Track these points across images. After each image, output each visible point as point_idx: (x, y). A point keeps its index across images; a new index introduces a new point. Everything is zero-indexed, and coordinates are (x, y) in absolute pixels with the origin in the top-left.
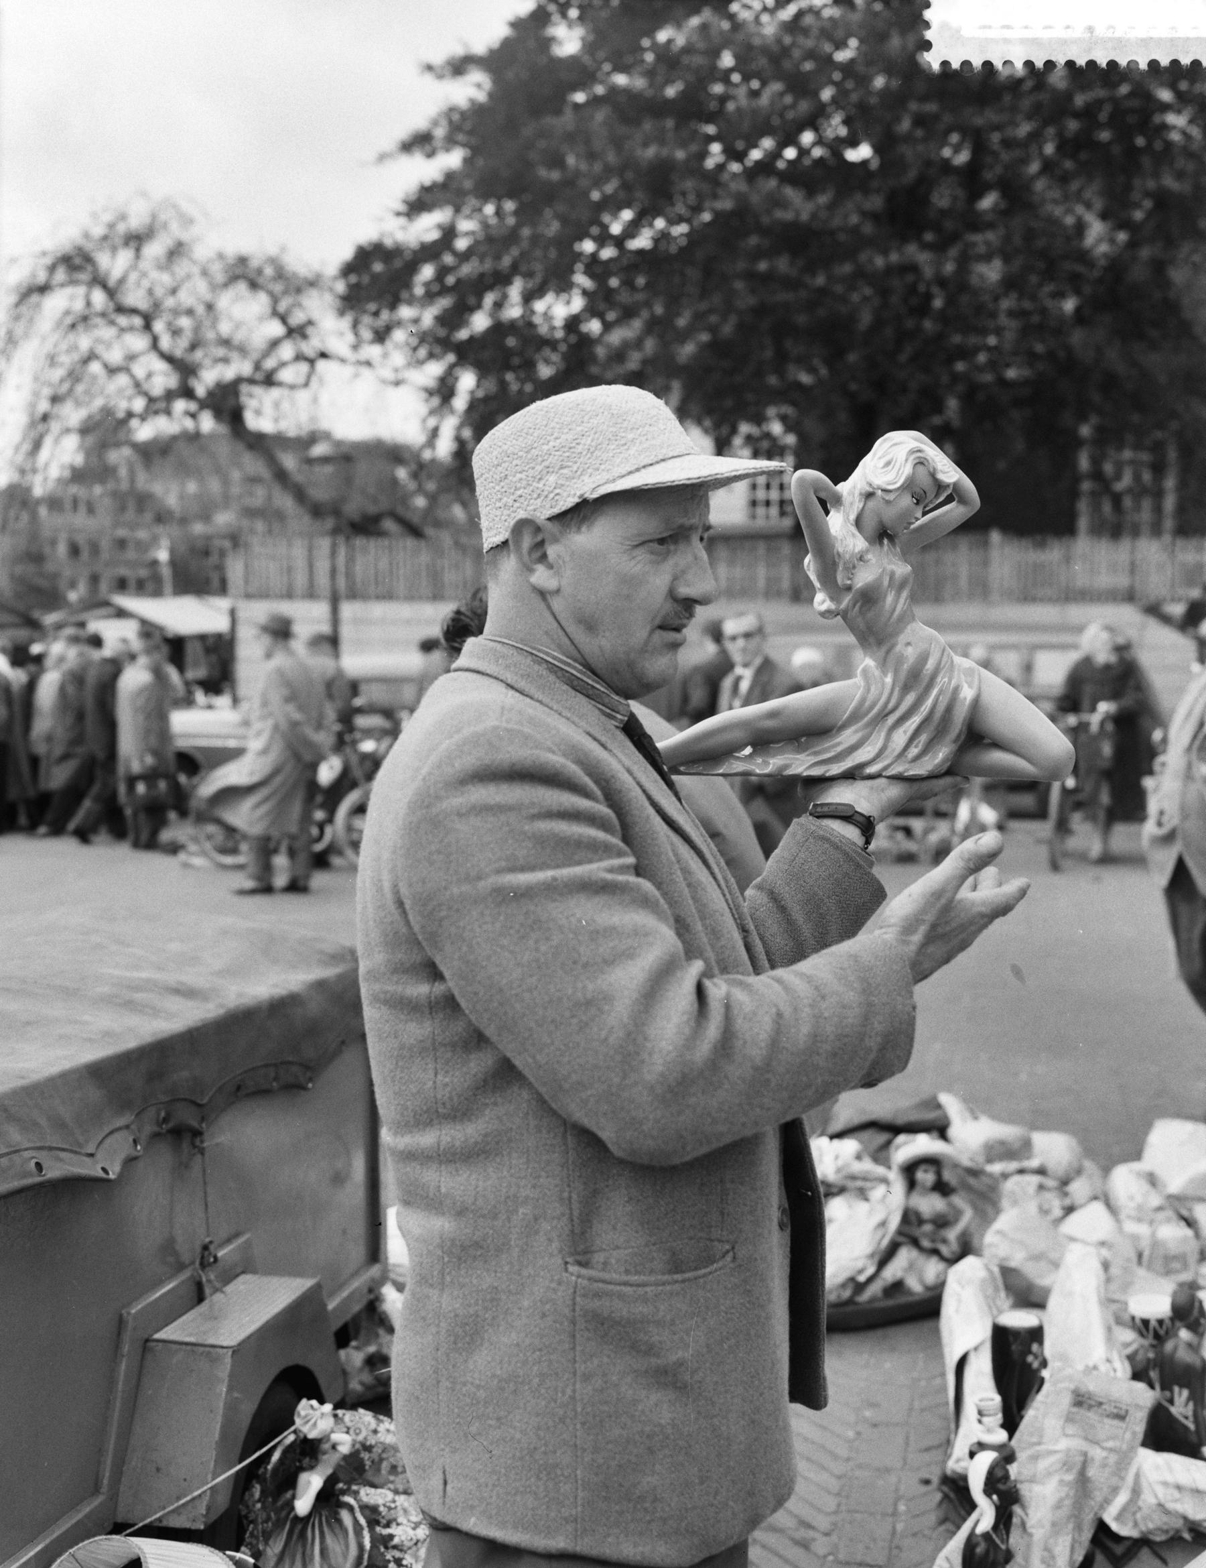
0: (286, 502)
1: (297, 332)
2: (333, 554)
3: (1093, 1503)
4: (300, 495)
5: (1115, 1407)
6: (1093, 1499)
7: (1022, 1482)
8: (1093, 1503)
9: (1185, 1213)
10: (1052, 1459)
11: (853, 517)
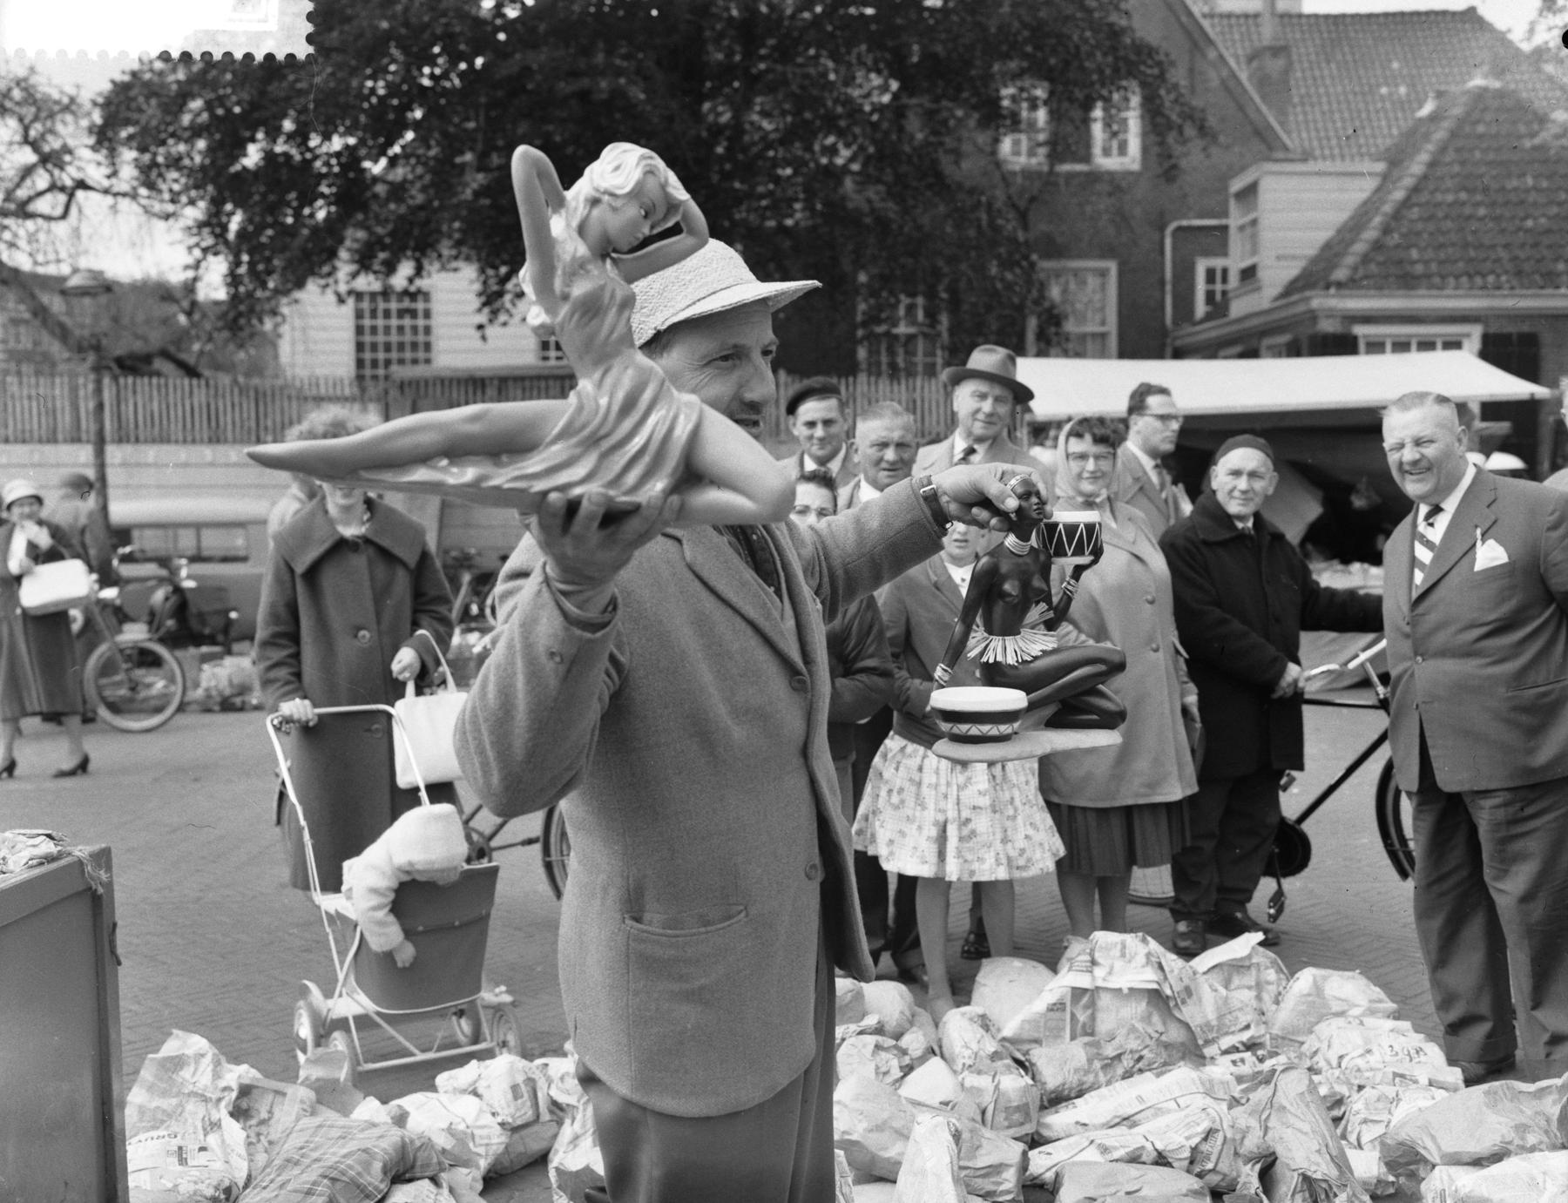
0: (55, 348)
1: (51, 160)
2: (98, 390)
4: (63, 334)
11: (575, 223)
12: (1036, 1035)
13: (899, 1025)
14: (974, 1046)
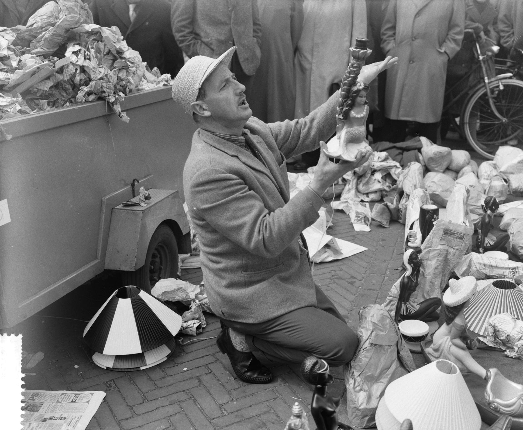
3: (449, 267)
5: (459, 235)
6: (449, 266)
7: (423, 260)
8: (449, 267)
9: (506, 178)
10: (435, 252)
12: (512, 171)
13: (463, 164)
14: (489, 173)
